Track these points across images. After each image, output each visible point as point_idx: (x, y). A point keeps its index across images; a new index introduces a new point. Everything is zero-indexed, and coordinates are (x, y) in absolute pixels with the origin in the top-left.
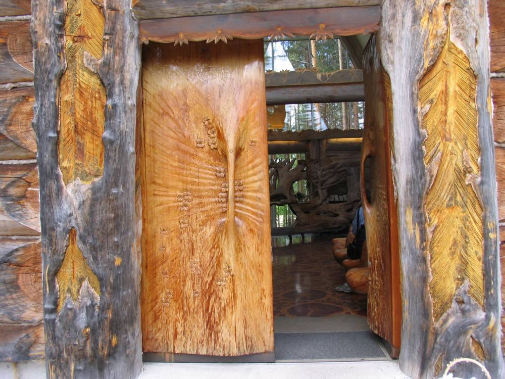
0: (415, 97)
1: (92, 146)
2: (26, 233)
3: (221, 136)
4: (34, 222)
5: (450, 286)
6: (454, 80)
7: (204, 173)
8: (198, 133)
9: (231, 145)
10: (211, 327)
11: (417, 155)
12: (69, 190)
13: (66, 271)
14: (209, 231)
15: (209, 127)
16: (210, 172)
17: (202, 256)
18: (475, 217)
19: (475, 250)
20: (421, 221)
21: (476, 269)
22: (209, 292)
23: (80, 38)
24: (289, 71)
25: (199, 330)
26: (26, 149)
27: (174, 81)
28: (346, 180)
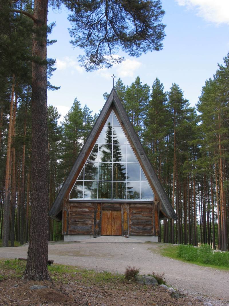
0: (123, 215)
1: (99, 217)
2: (92, 224)
3: (108, 217)
4: (93, 223)
5: (125, 229)
6: (126, 214)
7: (106, 220)
8: (106, 216)
9: (109, 218)
10: (107, 233)
11: (123, 219)
12: (97, 221)
13: (96, 227)
14: (107, 225)
15: (107, 216)
16: (210, 244)
17: (106, 227)
18: (127, 224)
19: (127, 226)
20: (123, 224)
21: (127, 228)
22: (106, 230)
23: (99, 209)
24: (72, 107)
25: (105, 233)
26: (92, 217)
27: (104, 212)
28: (149, 36)
